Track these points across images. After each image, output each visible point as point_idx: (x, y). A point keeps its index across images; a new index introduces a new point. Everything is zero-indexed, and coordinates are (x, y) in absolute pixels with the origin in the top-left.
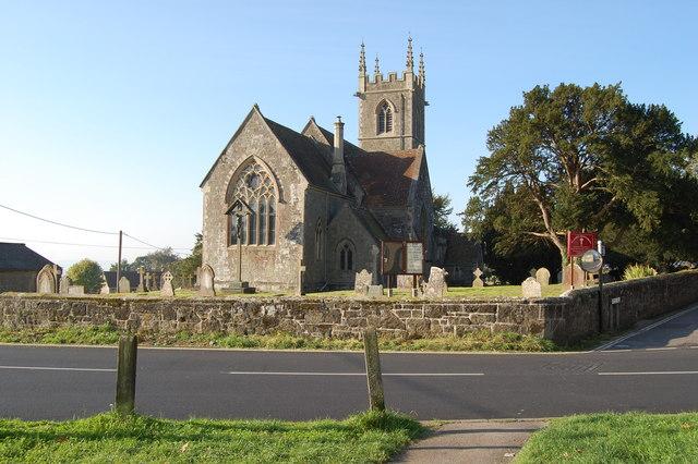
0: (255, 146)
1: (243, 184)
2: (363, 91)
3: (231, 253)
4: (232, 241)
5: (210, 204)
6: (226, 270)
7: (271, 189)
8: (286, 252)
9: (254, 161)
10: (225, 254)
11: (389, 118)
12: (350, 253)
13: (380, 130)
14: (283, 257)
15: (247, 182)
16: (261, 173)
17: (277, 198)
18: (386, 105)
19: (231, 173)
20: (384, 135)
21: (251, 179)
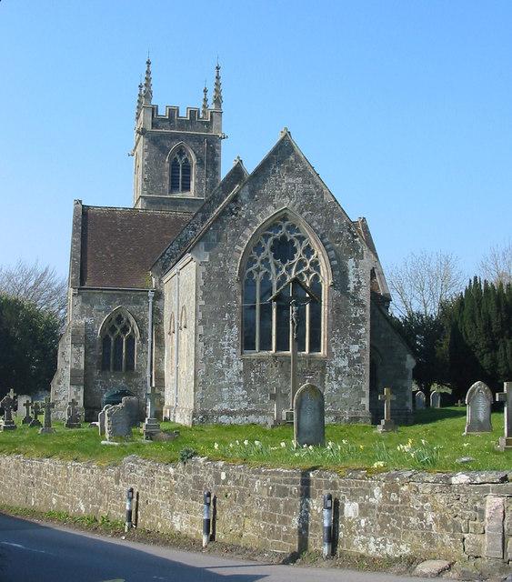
0: (288, 194)
1: (267, 253)
2: (149, 128)
3: (249, 366)
4: (248, 344)
5: (207, 281)
6: (240, 392)
7: (315, 265)
8: (343, 363)
9: (284, 219)
10: (238, 366)
11: (187, 170)
12: (131, 341)
13: (174, 187)
14: (339, 371)
15: (272, 249)
16: (298, 238)
17: (326, 279)
18: (181, 152)
19: (249, 233)
20: (178, 195)
21: (283, 250)
